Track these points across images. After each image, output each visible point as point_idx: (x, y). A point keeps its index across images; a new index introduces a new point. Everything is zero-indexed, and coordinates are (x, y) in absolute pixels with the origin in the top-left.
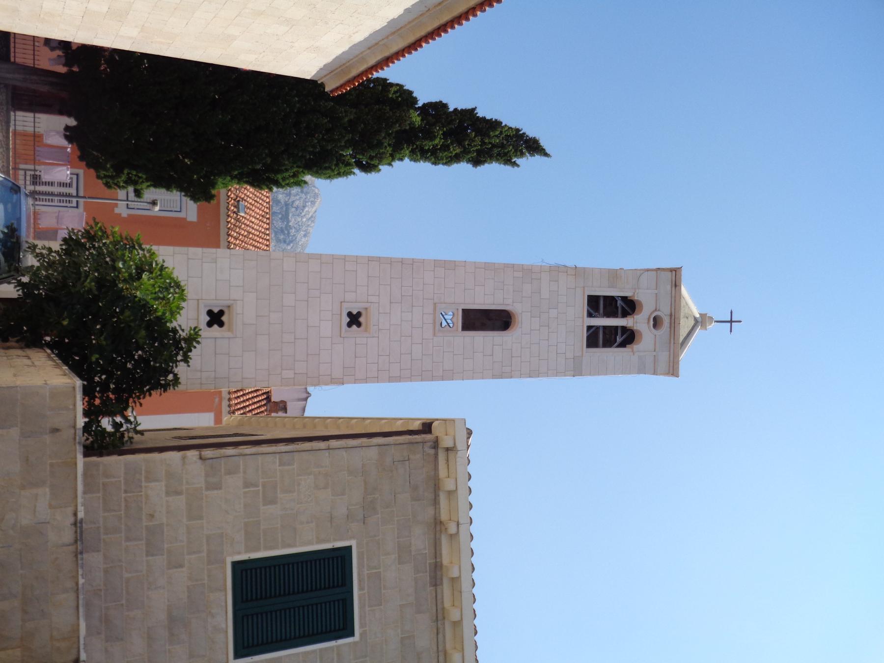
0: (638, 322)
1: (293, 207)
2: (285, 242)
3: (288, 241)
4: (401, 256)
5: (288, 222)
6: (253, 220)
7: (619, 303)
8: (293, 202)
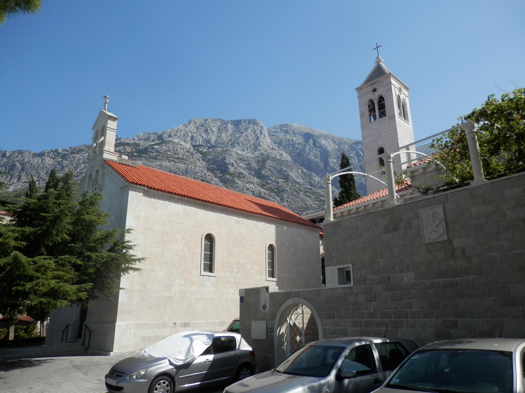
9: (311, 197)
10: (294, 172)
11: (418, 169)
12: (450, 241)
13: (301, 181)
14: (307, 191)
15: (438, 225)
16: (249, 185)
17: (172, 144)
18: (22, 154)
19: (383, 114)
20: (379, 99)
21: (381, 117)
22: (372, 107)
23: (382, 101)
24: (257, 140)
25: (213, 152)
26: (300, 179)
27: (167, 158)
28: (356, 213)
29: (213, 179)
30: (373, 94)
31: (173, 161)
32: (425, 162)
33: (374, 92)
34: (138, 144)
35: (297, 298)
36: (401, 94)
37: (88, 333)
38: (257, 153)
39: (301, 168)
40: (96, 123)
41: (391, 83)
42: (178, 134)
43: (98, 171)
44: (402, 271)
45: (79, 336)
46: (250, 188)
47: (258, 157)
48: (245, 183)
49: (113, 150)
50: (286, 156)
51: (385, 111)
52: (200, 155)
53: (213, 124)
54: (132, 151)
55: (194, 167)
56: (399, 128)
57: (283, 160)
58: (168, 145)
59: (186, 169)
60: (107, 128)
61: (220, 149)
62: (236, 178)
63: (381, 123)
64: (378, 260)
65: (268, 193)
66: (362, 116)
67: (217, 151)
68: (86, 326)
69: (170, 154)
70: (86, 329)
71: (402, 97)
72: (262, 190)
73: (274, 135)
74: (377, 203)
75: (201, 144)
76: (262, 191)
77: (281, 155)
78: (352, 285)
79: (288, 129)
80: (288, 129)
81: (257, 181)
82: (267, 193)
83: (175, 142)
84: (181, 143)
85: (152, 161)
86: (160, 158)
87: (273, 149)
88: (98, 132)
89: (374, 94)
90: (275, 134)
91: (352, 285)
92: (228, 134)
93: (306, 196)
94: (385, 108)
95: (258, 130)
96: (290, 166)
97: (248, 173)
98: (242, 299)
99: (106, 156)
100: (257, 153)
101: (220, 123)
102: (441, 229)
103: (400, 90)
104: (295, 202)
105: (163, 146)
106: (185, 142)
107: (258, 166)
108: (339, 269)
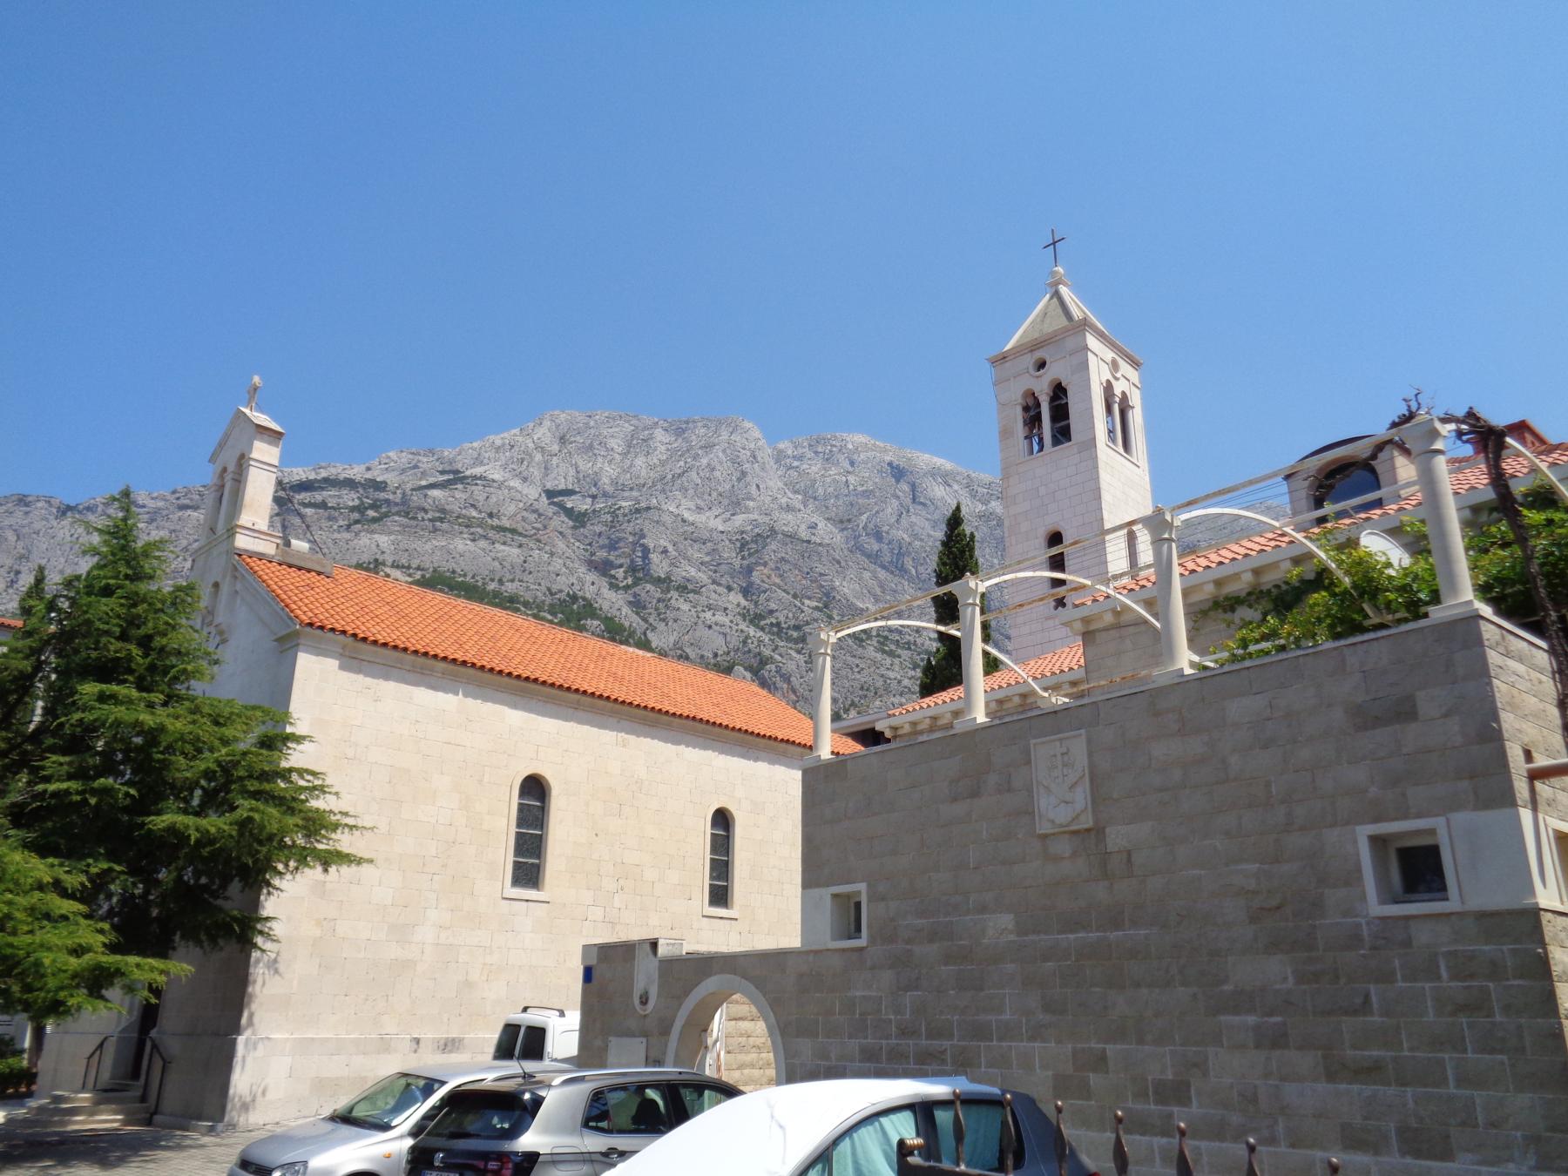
9: (899, 656)
10: (848, 578)
11: (1278, 562)
12: (1097, 831)
13: (870, 606)
14: (886, 638)
15: (1072, 787)
16: (714, 615)
17: (484, 486)
18: (27, 505)
19: (1063, 434)
20: (1054, 392)
21: (1056, 442)
22: (1032, 413)
23: (1061, 398)
24: (739, 480)
25: (609, 513)
26: (866, 600)
27: (467, 526)
28: (931, 730)
29: (605, 596)
30: (1038, 377)
31: (486, 538)
32: (1143, 586)
33: (1039, 370)
34: (381, 482)
35: (728, 976)
36: (1117, 379)
37: (158, 1064)
38: (739, 520)
39: (873, 567)
40: (221, 445)
41: (1086, 348)
42: (503, 458)
43: (216, 585)
44: (983, 909)
45: (135, 1074)
46: (716, 624)
47: (742, 532)
48: (700, 609)
49: (263, 525)
50: (827, 532)
51: (1068, 426)
52: (566, 520)
53: (610, 430)
54: (362, 503)
55: (547, 556)
56: (1105, 477)
57: (818, 541)
58: (474, 488)
59: (525, 562)
60: (252, 463)
61: (630, 503)
62: (674, 594)
63: (1057, 461)
64: (930, 877)
65: (770, 640)
66: (1005, 433)
67: (619, 509)
68: (155, 1046)
69: (477, 516)
70: (155, 1050)
71: (1119, 388)
72: (752, 631)
73: (791, 467)
74: (1008, 699)
75: (570, 487)
76: (752, 634)
77: (814, 526)
78: (862, 942)
79: (834, 449)
80: (834, 449)
81: (738, 605)
82: (767, 640)
83: (494, 481)
84: (512, 484)
85: (422, 537)
86: (445, 526)
87: (789, 508)
88: (225, 470)
89: (1040, 376)
90: (796, 464)
91: (862, 942)
92: (655, 461)
93: (884, 652)
94: (1068, 418)
95: (744, 449)
96: (839, 562)
97: (710, 577)
98: (588, 974)
99: (242, 541)
100: (739, 520)
101: (633, 428)
102: (1081, 797)
103: (1115, 366)
104: (851, 669)
105: (456, 492)
106: (525, 480)
107: (743, 558)
108: (835, 896)
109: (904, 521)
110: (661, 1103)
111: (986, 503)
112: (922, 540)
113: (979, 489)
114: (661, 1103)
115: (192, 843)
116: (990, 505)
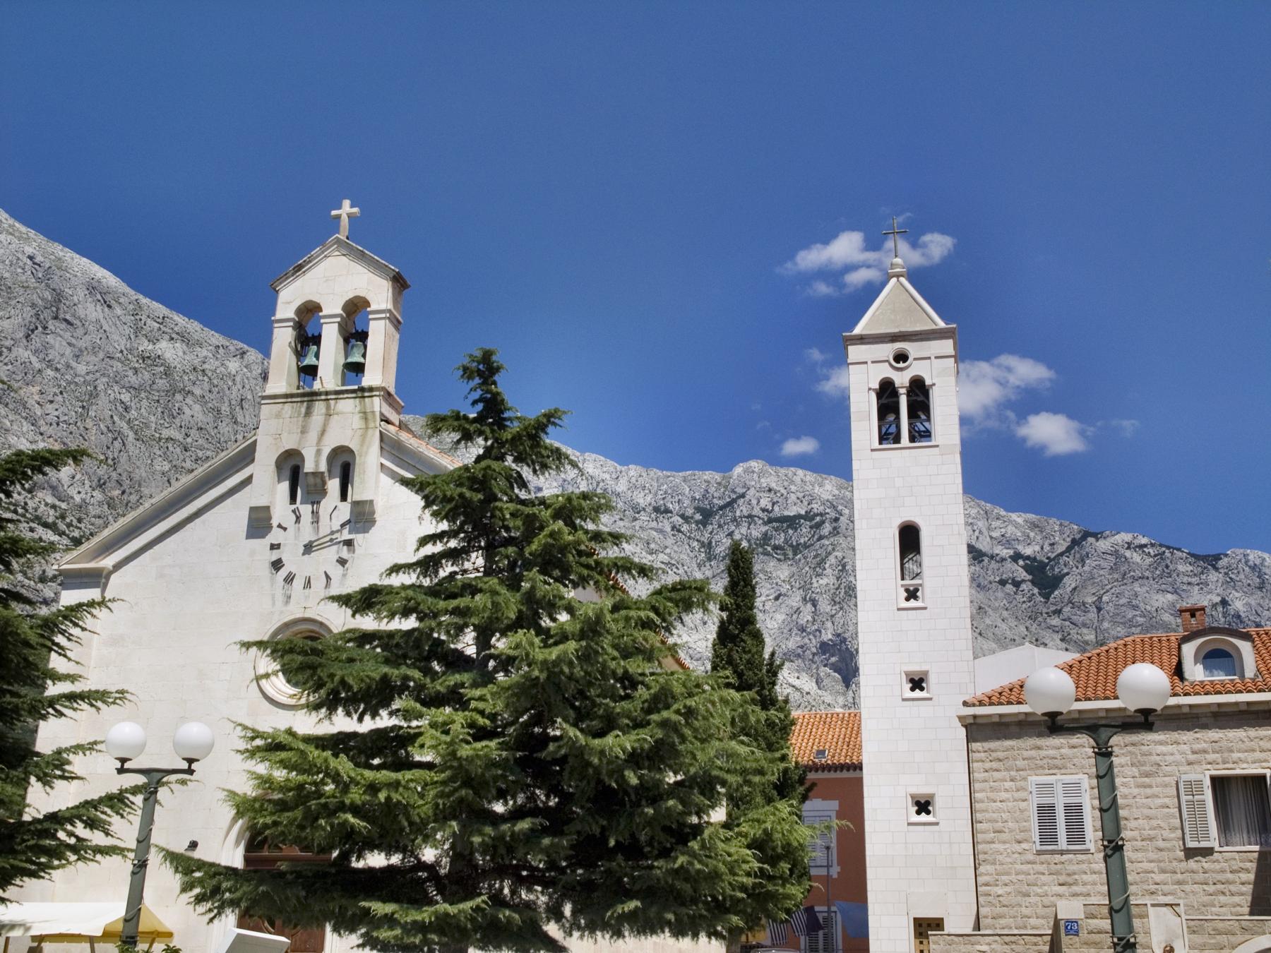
0: (902, 380)
1: (773, 510)
2: (836, 520)
3: (833, 515)
4: (860, 586)
5: (799, 516)
6: (830, 737)
7: (884, 401)
8: (763, 510)
60: (322, 321)
109: (37, 339)
110: (851, 826)
111: (154, 341)
112: (57, 370)
113: (149, 322)
114: (851, 826)
115: (535, 755)
116: (157, 346)
